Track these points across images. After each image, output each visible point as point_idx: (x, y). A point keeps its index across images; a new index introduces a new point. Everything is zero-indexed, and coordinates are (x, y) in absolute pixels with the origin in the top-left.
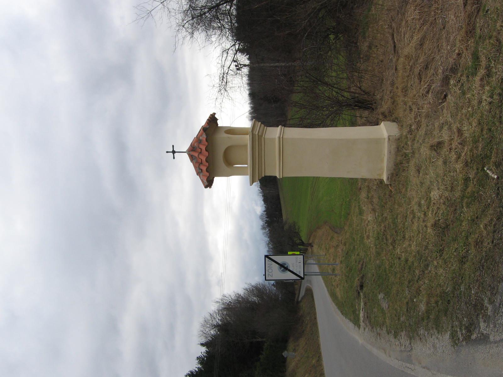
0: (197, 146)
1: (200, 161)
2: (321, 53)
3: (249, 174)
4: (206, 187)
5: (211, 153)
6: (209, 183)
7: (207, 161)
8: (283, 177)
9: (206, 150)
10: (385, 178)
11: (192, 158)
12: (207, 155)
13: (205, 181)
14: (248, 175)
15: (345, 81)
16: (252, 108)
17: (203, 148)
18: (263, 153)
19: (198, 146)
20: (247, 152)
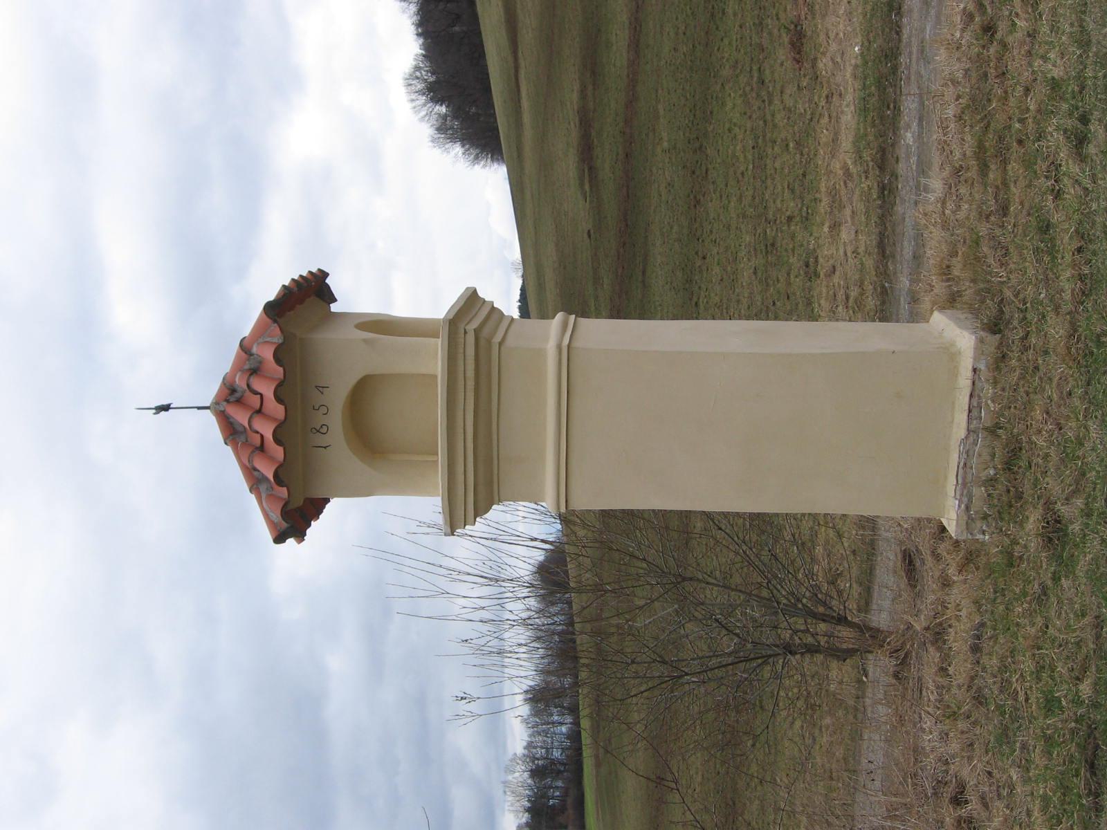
0: (245, 387)
1: (258, 442)
2: (674, 231)
3: (441, 495)
4: (280, 538)
5: (302, 404)
6: (294, 520)
7: (278, 359)
8: (571, 508)
9: (279, 399)
10: (951, 521)
11: (231, 432)
12: (281, 376)
13: (276, 516)
14: (439, 496)
15: (794, 691)
16: (426, 47)
17: (267, 390)
18: (495, 437)
19: (248, 386)
20: (438, 477)
